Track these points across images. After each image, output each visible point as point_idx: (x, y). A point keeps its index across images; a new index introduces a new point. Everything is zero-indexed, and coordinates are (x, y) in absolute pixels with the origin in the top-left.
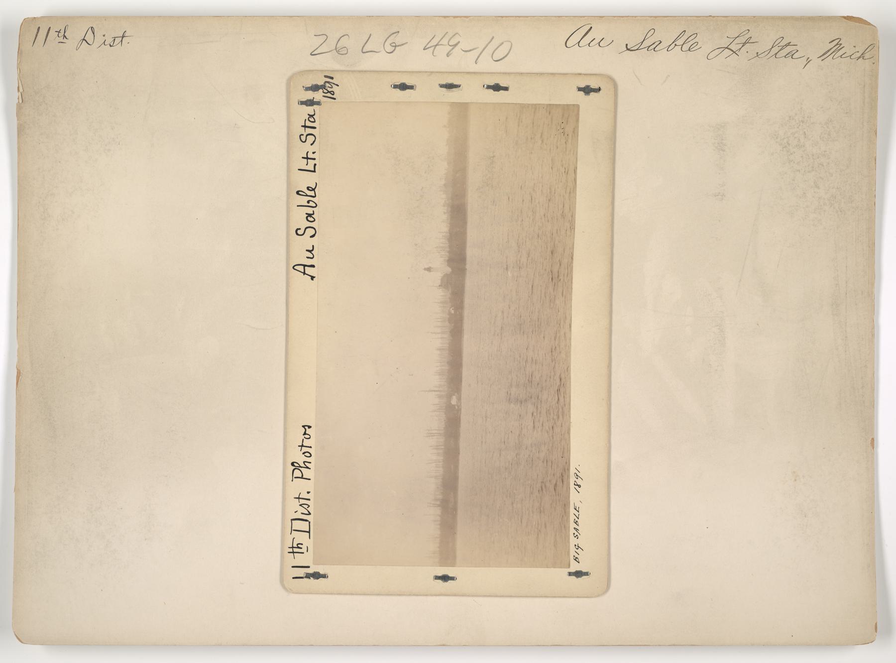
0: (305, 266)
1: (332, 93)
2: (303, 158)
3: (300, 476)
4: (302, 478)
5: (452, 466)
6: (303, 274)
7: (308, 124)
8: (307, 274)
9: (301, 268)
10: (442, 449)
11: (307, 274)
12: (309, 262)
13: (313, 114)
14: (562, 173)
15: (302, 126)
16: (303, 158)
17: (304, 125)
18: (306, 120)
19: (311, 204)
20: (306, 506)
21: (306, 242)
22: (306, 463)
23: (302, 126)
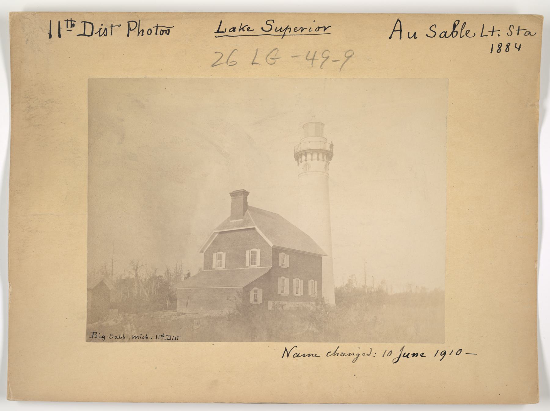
0: (401, 31)
1: (499, 51)
2: (519, 27)
3: (400, 32)
4: (394, 31)
5: (165, 278)
6: (111, 26)
7: (159, 29)
8: (112, 29)
9: (398, 28)
10: (291, 282)
11: (112, 29)
12: (405, 34)
13: (531, 34)
14: (142, 288)
15: (157, 24)
16: (519, 27)
17: (158, 26)
18: (247, 25)
19: (455, 34)
20: (105, 33)
21: (422, 30)
22: (142, 31)
23: (157, 24)
